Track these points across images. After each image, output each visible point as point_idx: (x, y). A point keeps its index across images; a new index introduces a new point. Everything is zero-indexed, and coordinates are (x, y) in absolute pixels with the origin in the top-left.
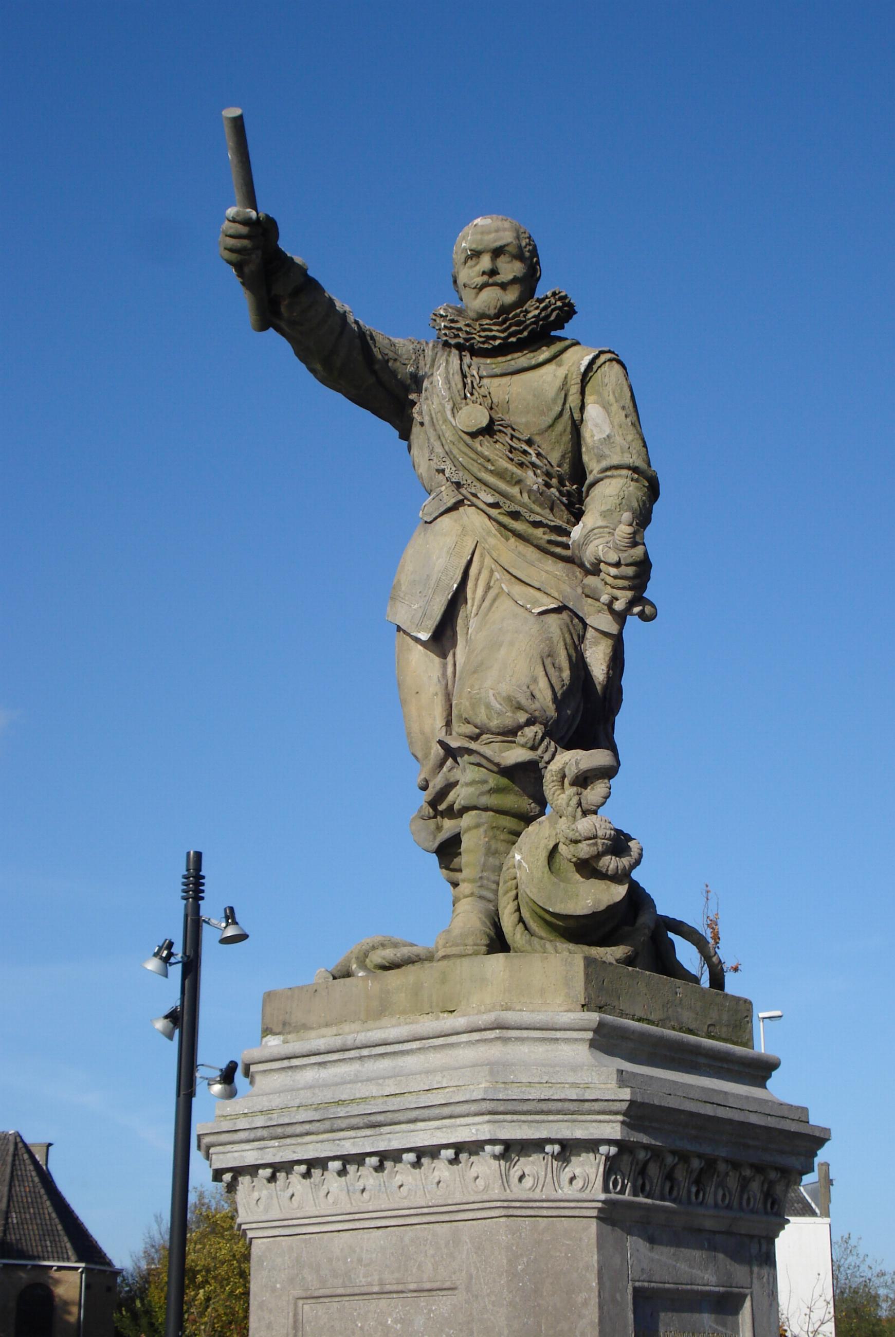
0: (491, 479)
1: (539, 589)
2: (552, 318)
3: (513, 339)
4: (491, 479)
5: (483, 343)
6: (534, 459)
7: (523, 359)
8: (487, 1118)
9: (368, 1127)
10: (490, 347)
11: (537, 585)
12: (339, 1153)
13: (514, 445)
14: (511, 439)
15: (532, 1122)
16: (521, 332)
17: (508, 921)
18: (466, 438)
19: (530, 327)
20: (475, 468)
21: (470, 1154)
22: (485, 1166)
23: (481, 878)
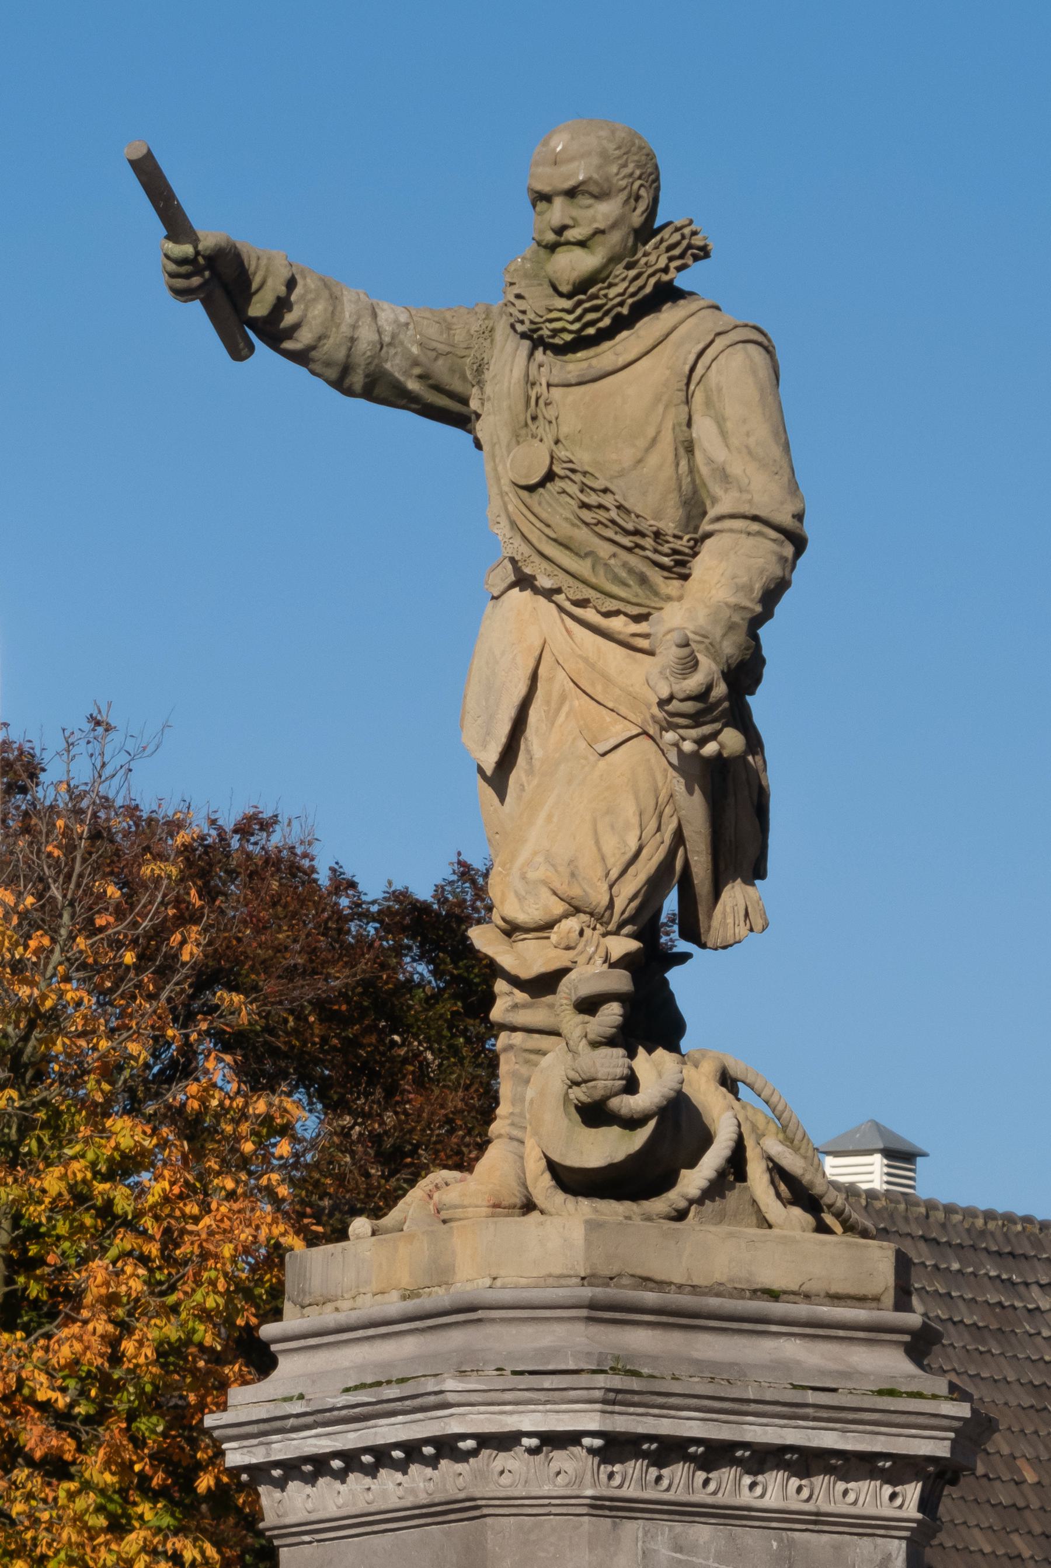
0: (551, 550)
1: (612, 710)
2: (648, 290)
3: (591, 331)
4: (551, 550)
6: (613, 514)
7: (352, 1436)
8: (598, 1406)
9: (745, 517)
10: (561, 342)
11: (610, 705)
12: (370, 1443)
13: (586, 500)
14: (582, 491)
15: (548, 1411)
16: (600, 319)
19: (624, 282)
20: (534, 536)
21: (377, 1214)
22: (569, 1462)
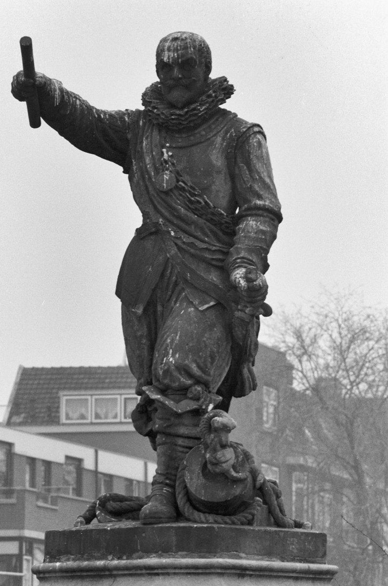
5: (173, 126)
17: (181, 501)
18: (163, 196)
23: (167, 473)
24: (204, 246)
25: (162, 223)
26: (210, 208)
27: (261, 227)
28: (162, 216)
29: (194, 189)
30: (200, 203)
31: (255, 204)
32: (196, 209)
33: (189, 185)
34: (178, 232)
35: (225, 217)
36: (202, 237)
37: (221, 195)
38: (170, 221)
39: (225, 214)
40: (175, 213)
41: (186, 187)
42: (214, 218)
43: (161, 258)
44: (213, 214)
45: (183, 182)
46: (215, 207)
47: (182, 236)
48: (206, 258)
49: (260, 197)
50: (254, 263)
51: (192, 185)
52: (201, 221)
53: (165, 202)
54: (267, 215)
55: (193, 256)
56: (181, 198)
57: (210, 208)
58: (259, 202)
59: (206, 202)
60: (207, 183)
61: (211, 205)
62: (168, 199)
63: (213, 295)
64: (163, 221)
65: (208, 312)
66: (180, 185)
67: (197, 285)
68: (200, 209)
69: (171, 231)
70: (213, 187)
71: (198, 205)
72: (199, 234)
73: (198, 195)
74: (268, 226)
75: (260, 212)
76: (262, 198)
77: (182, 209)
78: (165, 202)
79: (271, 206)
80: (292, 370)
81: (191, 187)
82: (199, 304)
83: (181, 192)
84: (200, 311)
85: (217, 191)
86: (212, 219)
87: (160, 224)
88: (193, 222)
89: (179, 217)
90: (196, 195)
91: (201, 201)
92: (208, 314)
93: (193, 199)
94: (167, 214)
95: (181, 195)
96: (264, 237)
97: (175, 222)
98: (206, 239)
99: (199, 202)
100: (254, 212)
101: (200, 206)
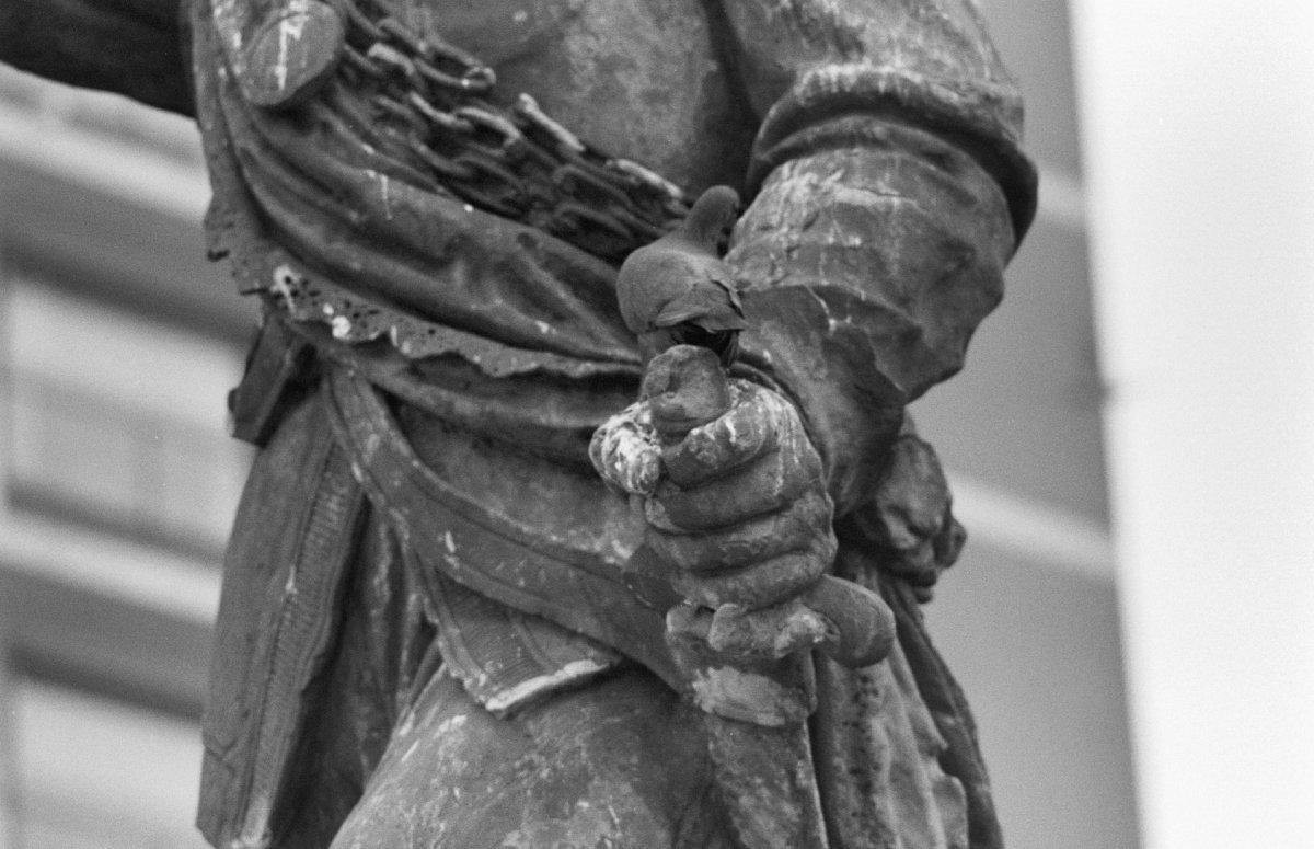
18: (281, 136)
24: (528, 362)
25: (285, 289)
26: (563, 160)
27: (844, 194)
28: (297, 253)
29: (459, 69)
30: (497, 136)
31: (815, 83)
32: (481, 178)
33: (422, 46)
34: (373, 313)
35: (675, 206)
36: (519, 319)
37: (635, 84)
38: (339, 275)
39: (674, 190)
40: (354, 216)
41: (409, 66)
42: (602, 217)
43: (333, 505)
44: (582, 190)
45: (394, 41)
46: (591, 153)
47: (394, 333)
48: (552, 431)
49: (846, 44)
50: (768, 368)
51: (442, 46)
52: (499, 232)
53: (295, 168)
54: (893, 135)
55: (489, 440)
56: (392, 132)
57: (563, 160)
58: (836, 72)
59: (531, 129)
60: (531, 19)
61: (570, 140)
62: (310, 148)
63: (586, 623)
64: (296, 278)
65: (548, 718)
66: (376, 60)
67: (493, 591)
68: (501, 172)
69: (337, 313)
70: (575, 44)
71: (483, 148)
72: (496, 304)
73: (484, 96)
74: (894, 185)
75: (849, 122)
76: (861, 48)
77: (384, 179)
78: (295, 168)
79: (917, 79)
80: (515, 829)
81: (440, 60)
82: (493, 680)
83: (385, 101)
84: (493, 714)
85: (607, 66)
86: (588, 225)
87: (279, 296)
88: (460, 246)
89: (380, 236)
90: (467, 97)
91: (502, 122)
92: (546, 727)
93: (446, 118)
94: (310, 233)
95: (387, 117)
96: (857, 241)
97: (356, 266)
98: (544, 327)
99: (486, 133)
100: (811, 132)
101: (497, 153)
